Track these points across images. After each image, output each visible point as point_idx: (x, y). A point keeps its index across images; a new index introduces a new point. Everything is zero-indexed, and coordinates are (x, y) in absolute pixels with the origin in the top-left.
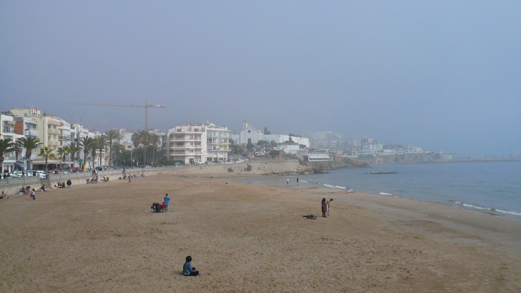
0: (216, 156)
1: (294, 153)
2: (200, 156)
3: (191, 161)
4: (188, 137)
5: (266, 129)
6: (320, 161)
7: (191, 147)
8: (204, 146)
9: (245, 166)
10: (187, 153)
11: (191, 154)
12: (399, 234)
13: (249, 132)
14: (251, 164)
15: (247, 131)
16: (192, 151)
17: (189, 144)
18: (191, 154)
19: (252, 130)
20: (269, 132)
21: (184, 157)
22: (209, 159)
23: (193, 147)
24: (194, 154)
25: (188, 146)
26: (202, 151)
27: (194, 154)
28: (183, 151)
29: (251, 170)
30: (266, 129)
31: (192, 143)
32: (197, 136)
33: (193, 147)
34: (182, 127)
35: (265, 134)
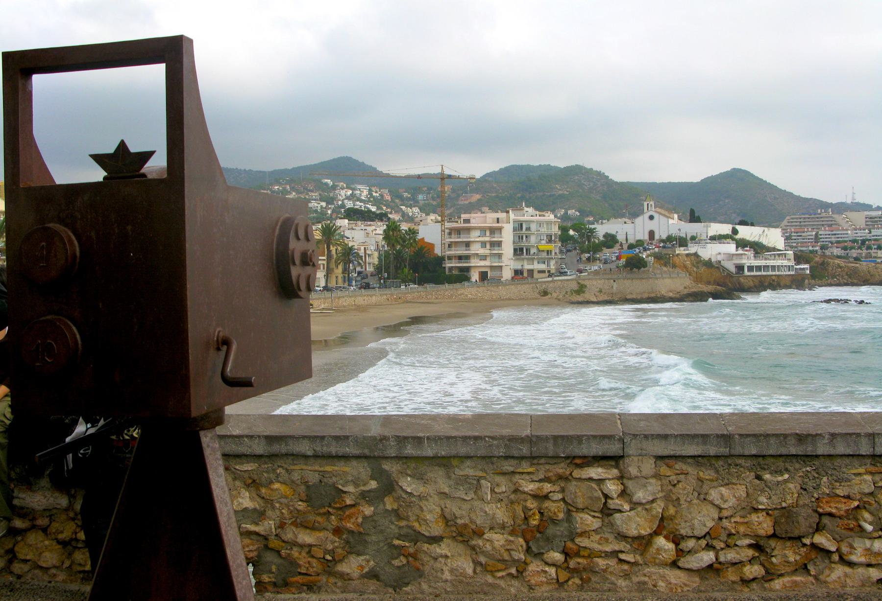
0: (530, 267)
1: (719, 258)
2: (501, 267)
3: (483, 276)
4: (478, 233)
5: (692, 212)
6: (770, 273)
7: (482, 251)
8: (508, 249)
9: (575, 286)
10: (474, 262)
11: (482, 263)
12: (862, 302)
13: (651, 218)
14: (586, 283)
15: (647, 216)
16: (484, 258)
17: (478, 246)
18: (482, 263)
19: (656, 216)
20: (699, 217)
21: (468, 269)
22: (518, 273)
23: (486, 251)
24: (487, 263)
25: (476, 249)
26: (504, 258)
27: (487, 263)
28: (467, 258)
29: (584, 292)
30: (692, 212)
31: (484, 244)
32: (493, 231)
33: (486, 251)
34: (473, 215)
35: (691, 221)
